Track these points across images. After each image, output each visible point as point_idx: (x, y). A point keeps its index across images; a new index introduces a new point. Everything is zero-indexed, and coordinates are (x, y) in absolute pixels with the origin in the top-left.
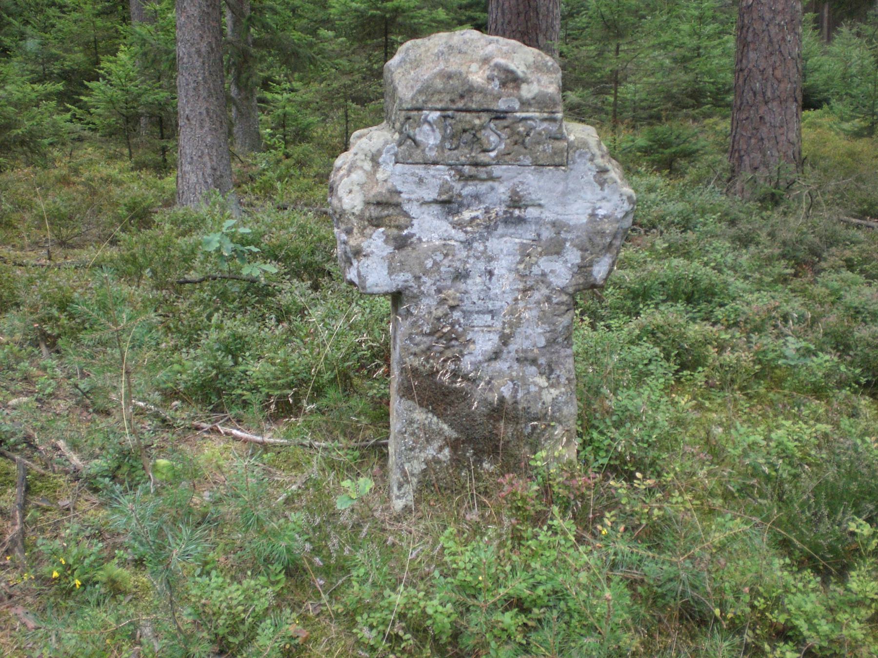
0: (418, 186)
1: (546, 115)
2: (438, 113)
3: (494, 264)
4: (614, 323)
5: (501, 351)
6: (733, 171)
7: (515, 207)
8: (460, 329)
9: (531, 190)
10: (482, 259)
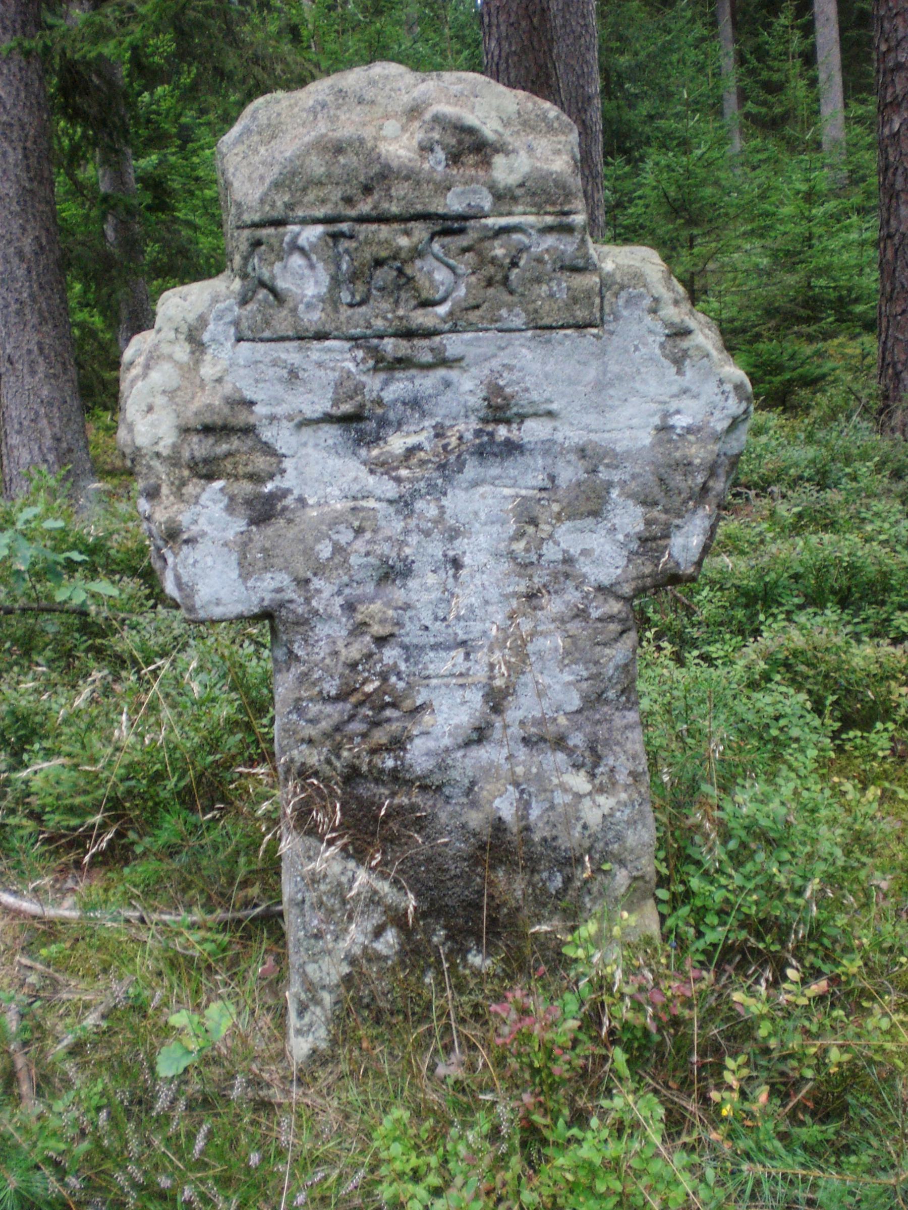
0: (289, 389)
1: (549, 220)
2: (320, 229)
3: (461, 545)
4: (714, 650)
5: (490, 725)
6: (886, 398)
7: (498, 421)
8: (401, 685)
9: (529, 382)
10: (436, 535)
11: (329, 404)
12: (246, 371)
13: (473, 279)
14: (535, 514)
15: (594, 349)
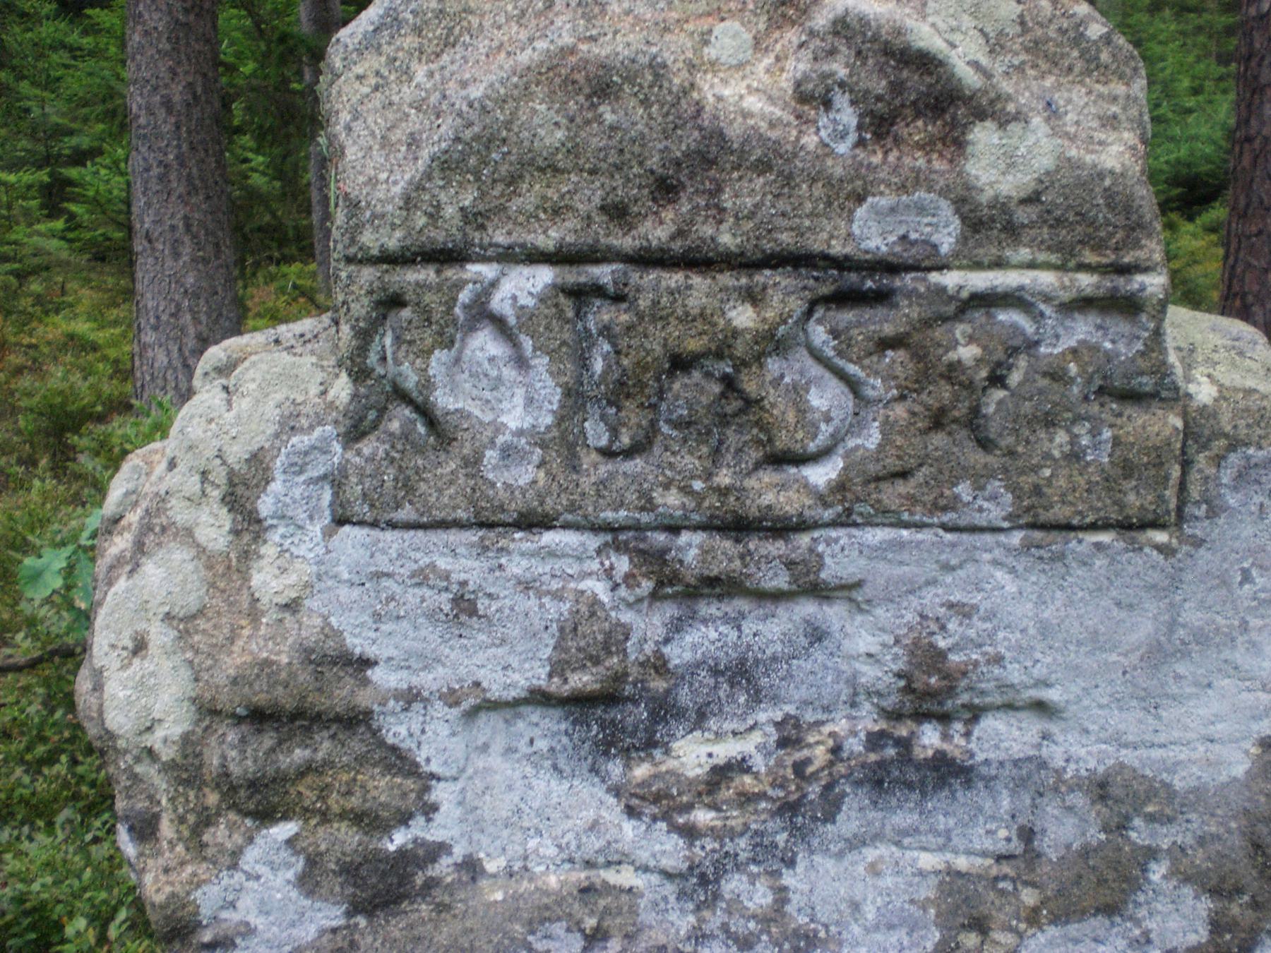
0: (453, 638)
1: (1086, 281)
2: (545, 275)
7: (921, 717)
9: (1004, 641)
11: (543, 672)
12: (356, 592)
13: (900, 411)
14: (984, 910)
15: (1154, 577)
